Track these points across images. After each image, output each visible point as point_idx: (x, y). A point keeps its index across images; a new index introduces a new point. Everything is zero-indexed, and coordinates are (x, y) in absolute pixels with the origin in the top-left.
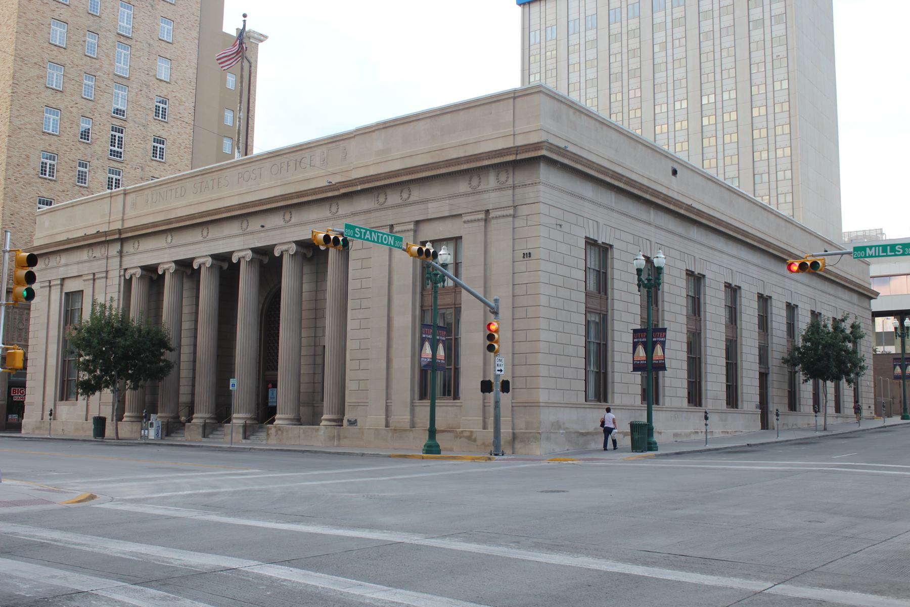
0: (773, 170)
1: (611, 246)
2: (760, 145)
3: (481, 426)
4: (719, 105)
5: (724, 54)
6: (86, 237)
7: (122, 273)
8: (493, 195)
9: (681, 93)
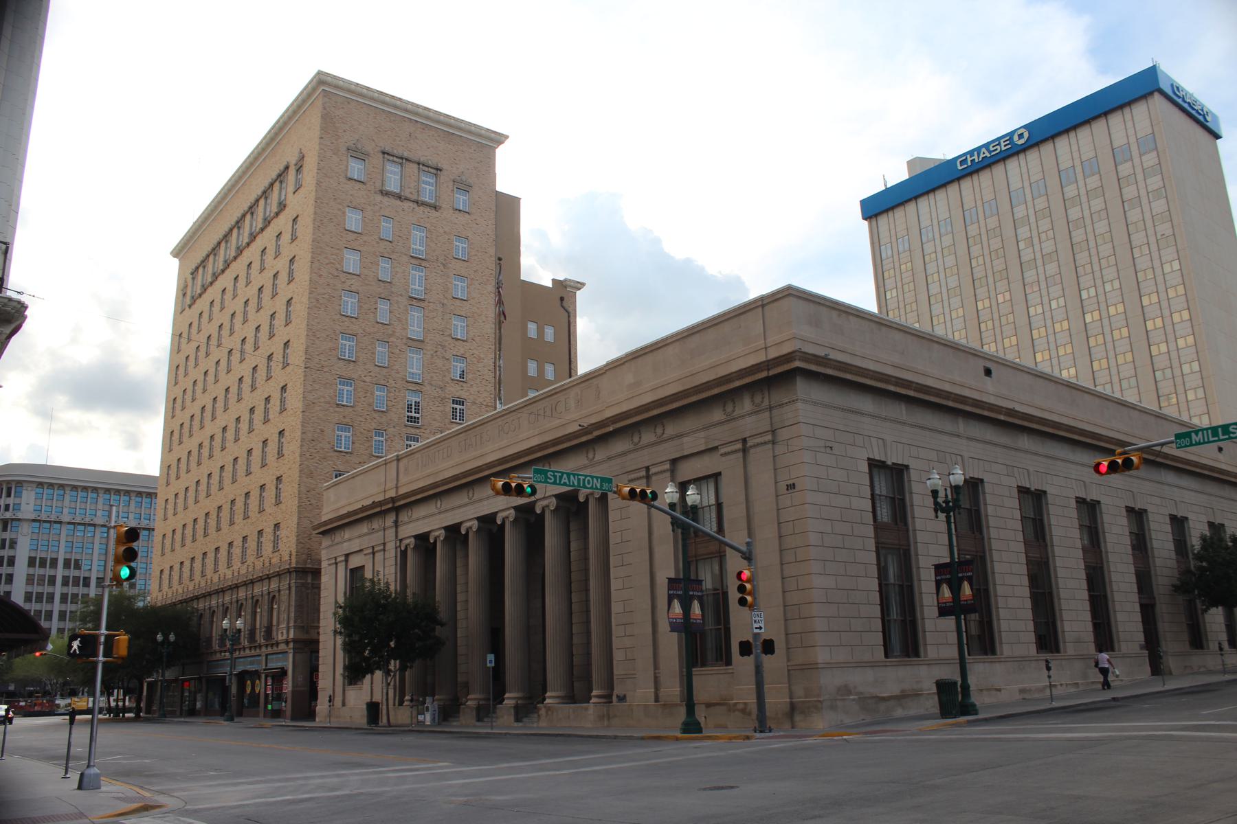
1: (907, 467)
5: (1100, 241)
6: (364, 509)
8: (749, 420)
9: (1056, 291)
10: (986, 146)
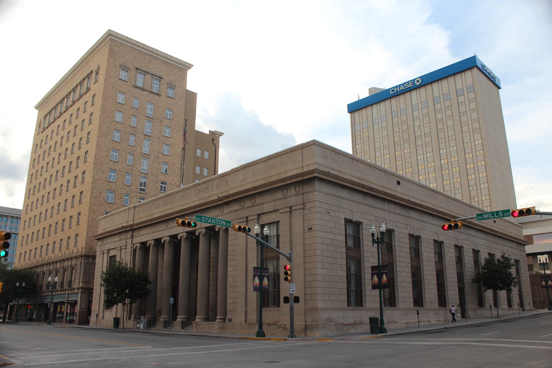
0: (478, 184)
2: (471, 172)
4: (449, 154)
6: (118, 229)
8: (293, 198)
9: (429, 149)
10: (403, 84)
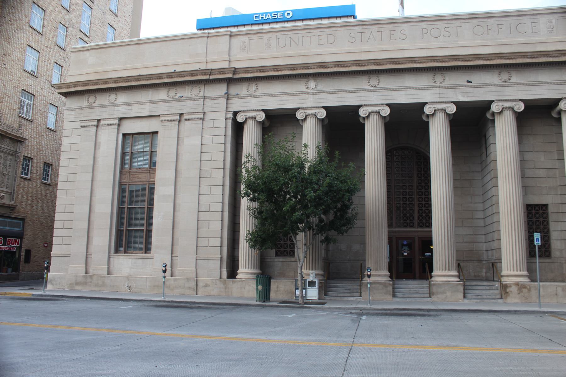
3: (219, 277)
7: (231, 115)
10: (271, 13)
